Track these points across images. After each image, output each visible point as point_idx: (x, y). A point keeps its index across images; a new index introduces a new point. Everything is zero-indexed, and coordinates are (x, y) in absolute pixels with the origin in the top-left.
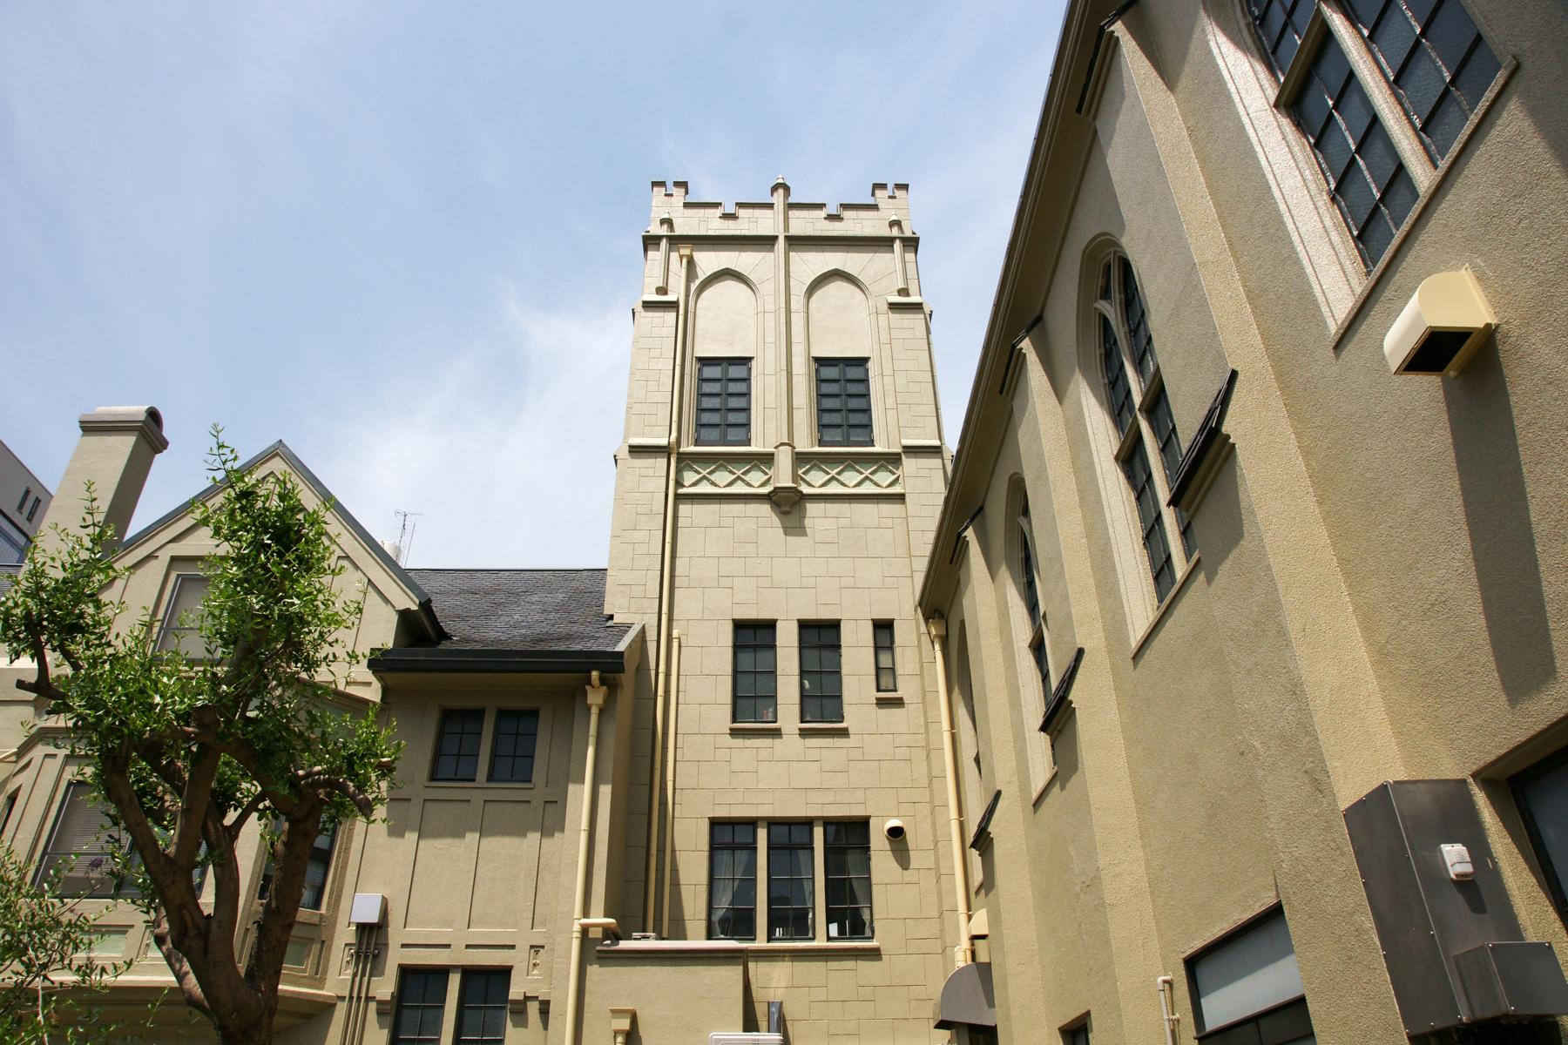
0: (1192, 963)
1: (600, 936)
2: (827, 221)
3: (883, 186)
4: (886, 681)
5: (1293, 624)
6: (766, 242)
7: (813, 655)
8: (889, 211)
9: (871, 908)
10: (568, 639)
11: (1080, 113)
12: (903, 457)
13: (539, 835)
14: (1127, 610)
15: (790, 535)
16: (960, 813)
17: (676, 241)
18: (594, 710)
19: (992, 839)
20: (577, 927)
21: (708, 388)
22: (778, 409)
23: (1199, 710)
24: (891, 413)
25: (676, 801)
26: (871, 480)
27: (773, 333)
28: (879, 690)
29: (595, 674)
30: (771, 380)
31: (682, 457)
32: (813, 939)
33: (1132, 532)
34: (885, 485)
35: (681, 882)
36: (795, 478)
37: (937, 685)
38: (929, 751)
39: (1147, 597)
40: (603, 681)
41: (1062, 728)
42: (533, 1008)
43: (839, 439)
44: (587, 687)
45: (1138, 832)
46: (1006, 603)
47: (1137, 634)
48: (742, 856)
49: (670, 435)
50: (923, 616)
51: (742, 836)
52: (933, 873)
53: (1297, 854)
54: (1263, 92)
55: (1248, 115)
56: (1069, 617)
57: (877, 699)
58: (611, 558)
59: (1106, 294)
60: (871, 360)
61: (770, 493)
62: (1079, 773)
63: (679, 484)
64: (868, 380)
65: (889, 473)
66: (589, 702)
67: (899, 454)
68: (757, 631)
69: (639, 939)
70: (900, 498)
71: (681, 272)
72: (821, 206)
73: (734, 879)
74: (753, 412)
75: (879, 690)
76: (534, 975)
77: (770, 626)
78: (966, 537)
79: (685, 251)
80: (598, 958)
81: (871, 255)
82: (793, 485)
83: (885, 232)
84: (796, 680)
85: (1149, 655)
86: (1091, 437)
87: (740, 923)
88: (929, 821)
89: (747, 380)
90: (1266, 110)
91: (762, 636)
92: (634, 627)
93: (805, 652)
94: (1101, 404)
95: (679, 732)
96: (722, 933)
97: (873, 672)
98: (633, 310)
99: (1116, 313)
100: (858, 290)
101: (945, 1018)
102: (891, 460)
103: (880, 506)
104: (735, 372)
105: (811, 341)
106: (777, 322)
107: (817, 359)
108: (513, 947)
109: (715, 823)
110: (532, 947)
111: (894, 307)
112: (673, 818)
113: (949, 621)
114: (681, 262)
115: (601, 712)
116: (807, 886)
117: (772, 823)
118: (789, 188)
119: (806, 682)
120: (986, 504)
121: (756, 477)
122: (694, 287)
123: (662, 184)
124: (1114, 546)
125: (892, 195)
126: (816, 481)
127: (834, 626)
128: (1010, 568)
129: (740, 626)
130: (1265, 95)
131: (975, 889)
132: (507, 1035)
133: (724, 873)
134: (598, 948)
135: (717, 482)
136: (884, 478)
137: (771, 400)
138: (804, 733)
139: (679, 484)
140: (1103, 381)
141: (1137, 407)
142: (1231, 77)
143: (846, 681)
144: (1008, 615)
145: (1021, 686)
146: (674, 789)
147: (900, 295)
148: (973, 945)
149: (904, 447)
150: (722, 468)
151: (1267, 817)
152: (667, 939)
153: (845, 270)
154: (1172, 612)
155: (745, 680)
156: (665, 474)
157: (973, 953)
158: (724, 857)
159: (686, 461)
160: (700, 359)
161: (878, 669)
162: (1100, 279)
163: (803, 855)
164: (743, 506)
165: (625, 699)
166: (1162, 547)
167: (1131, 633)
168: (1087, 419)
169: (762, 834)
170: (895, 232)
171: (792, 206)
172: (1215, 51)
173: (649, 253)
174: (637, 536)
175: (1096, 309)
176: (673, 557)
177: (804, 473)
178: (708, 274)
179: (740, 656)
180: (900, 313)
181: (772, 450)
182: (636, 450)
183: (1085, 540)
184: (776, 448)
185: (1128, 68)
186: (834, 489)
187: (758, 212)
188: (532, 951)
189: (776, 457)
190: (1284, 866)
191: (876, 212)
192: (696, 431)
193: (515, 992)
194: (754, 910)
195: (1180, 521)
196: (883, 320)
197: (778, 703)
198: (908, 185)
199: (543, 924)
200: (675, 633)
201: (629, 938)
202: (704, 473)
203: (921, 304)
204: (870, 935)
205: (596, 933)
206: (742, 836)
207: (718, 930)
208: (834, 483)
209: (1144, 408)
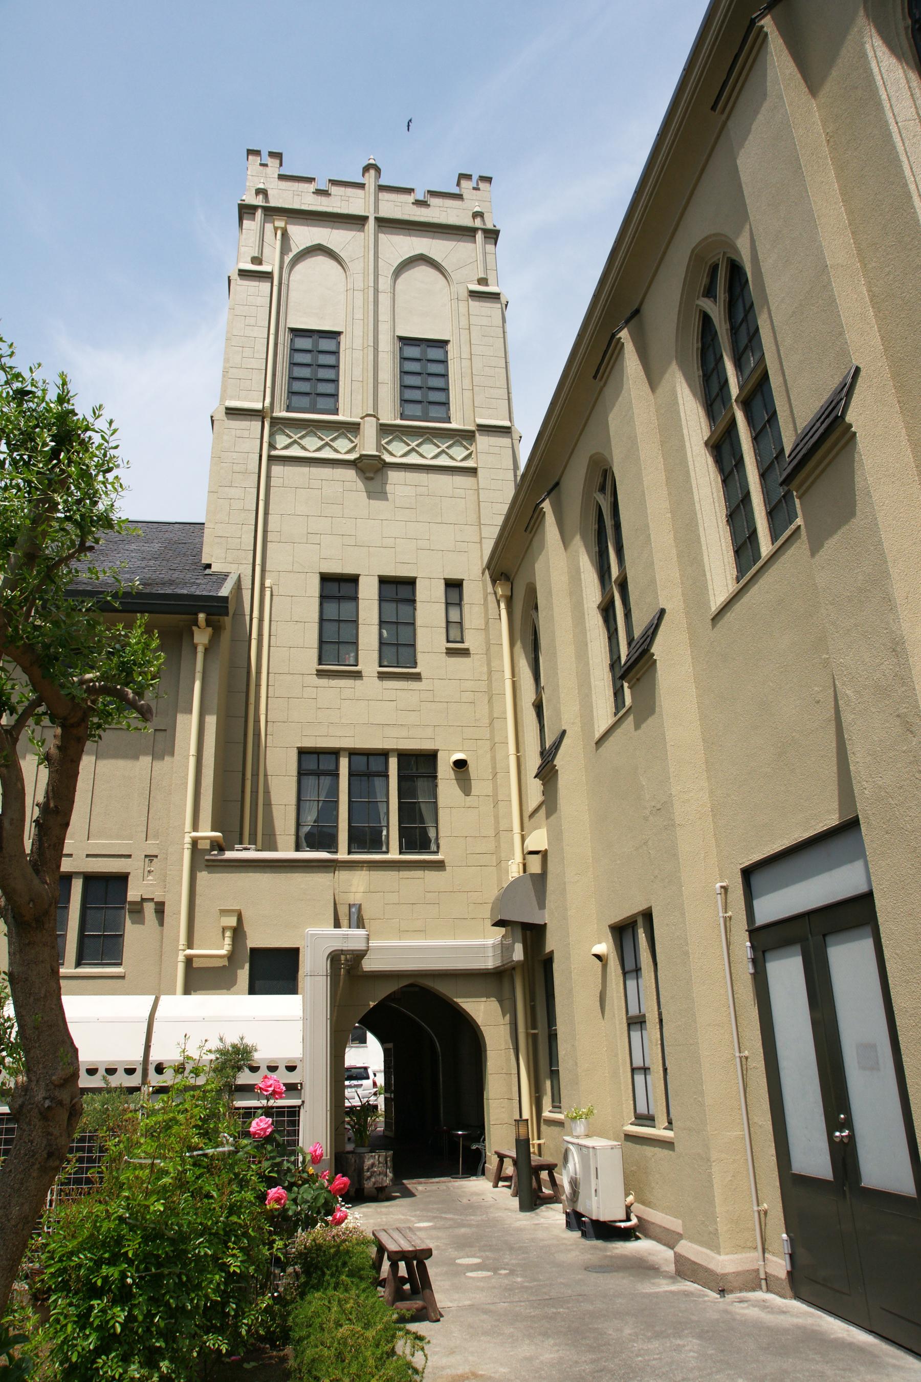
0: (747, 873)
1: (208, 847)
2: (415, 207)
3: (468, 177)
4: (454, 633)
5: (899, 591)
6: (356, 221)
7: (390, 607)
8: (473, 201)
9: (437, 827)
10: (171, 584)
11: (715, 111)
12: (477, 434)
13: (150, 758)
14: (708, 577)
15: (372, 499)
16: (518, 750)
17: (271, 212)
18: (200, 650)
19: (557, 771)
20: (187, 840)
21: (300, 358)
22: (365, 383)
23: (778, 665)
24: (468, 394)
25: (268, 733)
26: (447, 454)
27: (361, 310)
28: (448, 641)
29: (202, 616)
30: (358, 355)
31: (275, 422)
32: (387, 852)
33: (717, 511)
34: (459, 458)
35: (273, 802)
36: (379, 447)
37: (501, 639)
38: (491, 697)
39: (727, 567)
40: (208, 623)
41: (641, 676)
42: (149, 909)
43: (419, 413)
44: (194, 628)
45: (704, 767)
46: (579, 568)
47: (718, 598)
48: (326, 781)
49: (264, 399)
50: (491, 577)
51: (326, 764)
52: (491, 799)
53: (880, 783)
54: (914, 101)
55: (897, 123)
56: (653, 581)
57: (447, 649)
58: (208, 512)
59: (709, 292)
60: (451, 343)
61: (356, 459)
62: (656, 715)
63: (272, 446)
64: (447, 362)
65: (463, 448)
66: (195, 641)
67: (473, 432)
68: (341, 584)
69: (241, 850)
70: (473, 471)
71: (275, 243)
72: (409, 191)
73: (318, 801)
74: (341, 383)
75: (448, 641)
76: (149, 880)
77: (354, 580)
78: (543, 508)
79: (280, 223)
80: (207, 866)
81: (454, 243)
82: (377, 453)
83: (468, 222)
84: (375, 629)
85: (730, 616)
86: (684, 423)
87: (325, 840)
88: (489, 756)
89: (336, 353)
90: (914, 120)
91: (346, 589)
92: (231, 576)
93: (384, 604)
94: (695, 395)
95: (270, 671)
96: (308, 847)
97: (444, 625)
98: (229, 277)
99: (719, 311)
100: (441, 276)
101: (503, 918)
102: (466, 436)
103: (454, 477)
104: (325, 344)
105: (396, 320)
106: (365, 301)
107: (401, 339)
108: (129, 856)
109: (303, 752)
110: (146, 856)
111: (474, 294)
112: (266, 747)
113: (514, 584)
114: (276, 234)
115: (206, 650)
116: (382, 808)
117: (353, 753)
118: (380, 170)
119: (385, 632)
120: (562, 479)
121: (343, 445)
122: (287, 259)
123: (257, 153)
124: (700, 521)
125: (475, 186)
126: (397, 451)
127: (411, 582)
128: (584, 538)
129: (326, 578)
130: (915, 104)
131: (529, 814)
132: (126, 931)
133: (310, 795)
134: (207, 857)
135: (307, 447)
136: (459, 452)
137: (358, 373)
138: (382, 676)
139: (272, 446)
140: (698, 373)
141: (734, 397)
142: (884, 83)
143: (420, 632)
144: (580, 580)
145: (589, 641)
146: (267, 722)
147: (479, 284)
148: (524, 859)
149: (479, 426)
150: (312, 434)
151: (853, 753)
152: (261, 851)
153: (430, 256)
154: (757, 581)
155: (330, 628)
156: (259, 436)
157: (524, 865)
158: (311, 781)
159: (278, 425)
160: (292, 330)
161: (448, 622)
162: (705, 279)
163: (378, 782)
164: (331, 470)
165: (226, 636)
166: (745, 523)
167: (712, 598)
168: (681, 407)
169: (344, 763)
170: (478, 223)
171: (382, 188)
172: (870, 54)
173: (245, 222)
174: (233, 492)
175: (697, 306)
176: (266, 513)
177: (387, 443)
178: (301, 248)
179: (325, 605)
180: (479, 301)
181: (358, 420)
182: (232, 412)
183: (669, 515)
184: (362, 418)
185: (774, 67)
186: (413, 459)
187: (350, 191)
188: (147, 860)
189: (362, 426)
190: (866, 792)
191: (460, 202)
192: (288, 398)
193: (133, 894)
194: (337, 827)
195: (767, 502)
196: (463, 306)
197: (360, 648)
198: (491, 178)
199: (156, 837)
200: (268, 583)
201: (232, 849)
202: (296, 437)
203: (499, 294)
204: (436, 850)
205: (204, 845)
206: (326, 764)
207: (305, 844)
208: (414, 454)
209: (740, 399)
